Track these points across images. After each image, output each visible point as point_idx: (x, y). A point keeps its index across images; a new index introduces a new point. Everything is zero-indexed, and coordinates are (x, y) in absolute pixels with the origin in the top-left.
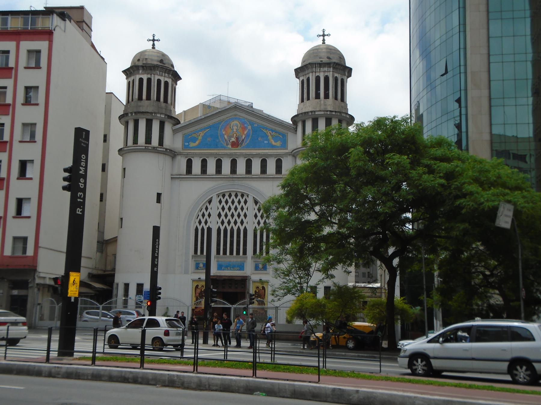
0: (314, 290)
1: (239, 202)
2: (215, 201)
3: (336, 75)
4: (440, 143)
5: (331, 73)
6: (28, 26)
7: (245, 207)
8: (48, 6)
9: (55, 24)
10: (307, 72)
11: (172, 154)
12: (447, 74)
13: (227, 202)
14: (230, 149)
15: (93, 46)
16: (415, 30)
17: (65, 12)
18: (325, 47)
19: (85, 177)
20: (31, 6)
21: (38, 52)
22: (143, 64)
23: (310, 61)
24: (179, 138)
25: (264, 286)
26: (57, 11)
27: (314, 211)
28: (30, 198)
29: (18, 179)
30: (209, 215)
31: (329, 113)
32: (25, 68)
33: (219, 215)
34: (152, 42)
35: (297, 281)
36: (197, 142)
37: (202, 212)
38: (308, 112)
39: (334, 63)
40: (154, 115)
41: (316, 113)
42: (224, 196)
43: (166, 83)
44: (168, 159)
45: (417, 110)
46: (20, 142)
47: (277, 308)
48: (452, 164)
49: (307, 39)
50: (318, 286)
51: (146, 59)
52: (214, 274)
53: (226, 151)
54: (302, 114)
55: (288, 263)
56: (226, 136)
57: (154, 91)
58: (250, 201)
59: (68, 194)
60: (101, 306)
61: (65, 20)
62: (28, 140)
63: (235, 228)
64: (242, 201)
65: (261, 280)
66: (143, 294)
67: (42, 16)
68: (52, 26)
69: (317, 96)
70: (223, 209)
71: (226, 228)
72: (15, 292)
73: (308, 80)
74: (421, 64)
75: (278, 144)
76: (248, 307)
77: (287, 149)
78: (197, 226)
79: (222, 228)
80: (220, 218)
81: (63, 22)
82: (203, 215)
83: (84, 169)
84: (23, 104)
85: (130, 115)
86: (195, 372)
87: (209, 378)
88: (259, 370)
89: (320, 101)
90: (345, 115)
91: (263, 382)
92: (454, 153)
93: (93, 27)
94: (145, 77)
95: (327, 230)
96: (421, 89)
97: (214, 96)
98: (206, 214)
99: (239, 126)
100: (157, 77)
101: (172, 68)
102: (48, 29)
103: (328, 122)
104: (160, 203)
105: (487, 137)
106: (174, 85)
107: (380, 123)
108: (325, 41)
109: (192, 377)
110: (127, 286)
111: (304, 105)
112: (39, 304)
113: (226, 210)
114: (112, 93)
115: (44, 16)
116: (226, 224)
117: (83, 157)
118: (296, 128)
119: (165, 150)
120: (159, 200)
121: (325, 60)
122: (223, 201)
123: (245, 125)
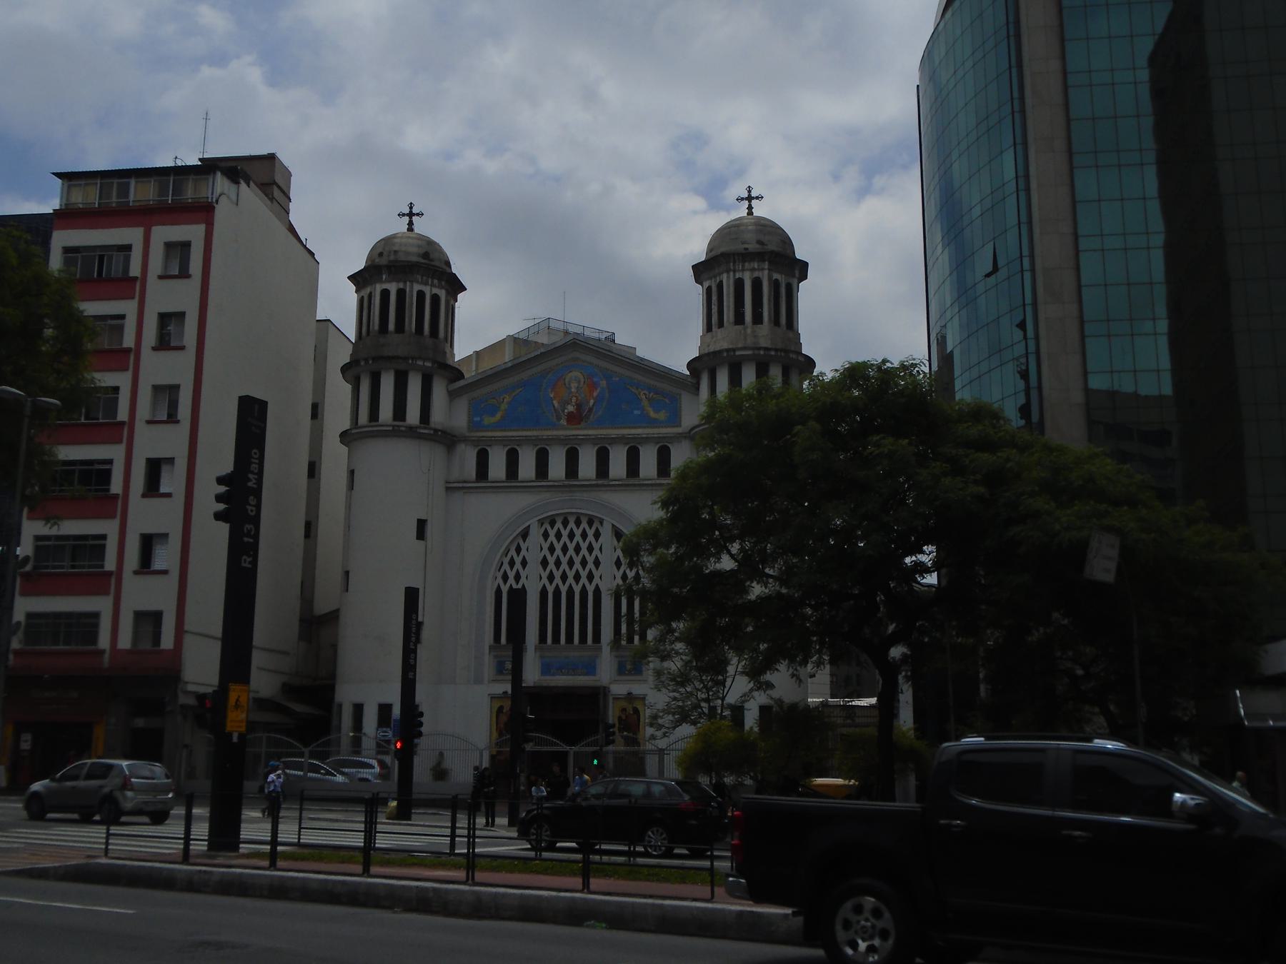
0: (738, 712)
1: (584, 535)
2: (536, 534)
3: (776, 276)
4: (980, 413)
5: (766, 272)
6: (168, 196)
7: (596, 546)
8: (206, 156)
9: (218, 190)
10: (717, 271)
11: (448, 440)
12: (998, 273)
13: (559, 535)
14: (564, 428)
15: (292, 230)
16: (932, 187)
17: (239, 168)
18: (753, 221)
19: (258, 492)
20: (176, 158)
21: (186, 246)
22: (390, 261)
23: (723, 249)
24: (462, 407)
25: (635, 705)
26: (223, 164)
27: (729, 552)
28: (168, 534)
29: (144, 496)
30: (524, 563)
31: (762, 352)
32: (161, 277)
33: (544, 563)
34: (407, 219)
35: (701, 695)
36: (498, 416)
37: (509, 556)
38: (720, 352)
39: (772, 252)
40: (410, 361)
41: (738, 353)
42: (552, 523)
43: (436, 299)
44: (439, 452)
45: (942, 342)
46: (149, 422)
47: (661, 752)
48: (999, 454)
49: (715, 205)
50: (747, 705)
51: (396, 252)
52: (535, 683)
53: (555, 433)
54: (708, 354)
55: (681, 659)
56: (556, 404)
57: (412, 315)
58: (606, 532)
59: (224, 528)
60: (306, 750)
61: (237, 183)
62: (165, 418)
63: (577, 589)
64: (590, 533)
65: (630, 694)
66: (392, 726)
67: (194, 177)
68: (212, 194)
69: (739, 319)
70: (552, 549)
71: (584, 589)
72: (140, 722)
73: (720, 286)
74: (946, 251)
75: (662, 416)
76: (601, 750)
77: (680, 426)
78: (499, 586)
79: (550, 589)
80: (545, 569)
81: (233, 187)
82: (512, 563)
83: (256, 477)
84: (154, 349)
85: (362, 363)
86: (470, 882)
87: (496, 894)
88: (594, 877)
89: (745, 329)
90: (794, 356)
91: (601, 900)
92: (1002, 433)
93: (293, 194)
94: (393, 288)
95: (757, 590)
96: (949, 303)
97: (537, 321)
98: (518, 560)
99: (582, 380)
100: (417, 287)
101: (447, 269)
102: (205, 200)
103: (762, 370)
104: (423, 540)
105: (1078, 397)
106: (452, 302)
107: (855, 373)
108: (753, 210)
109: (463, 892)
110: (358, 709)
111: (712, 338)
112: (186, 746)
113: (558, 552)
114: (329, 320)
115: (199, 177)
116: (558, 580)
117: (255, 453)
118: (698, 384)
119: (432, 432)
120: (421, 534)
121: (753, 247)
122: (552, 533)
123: (595, 380)
